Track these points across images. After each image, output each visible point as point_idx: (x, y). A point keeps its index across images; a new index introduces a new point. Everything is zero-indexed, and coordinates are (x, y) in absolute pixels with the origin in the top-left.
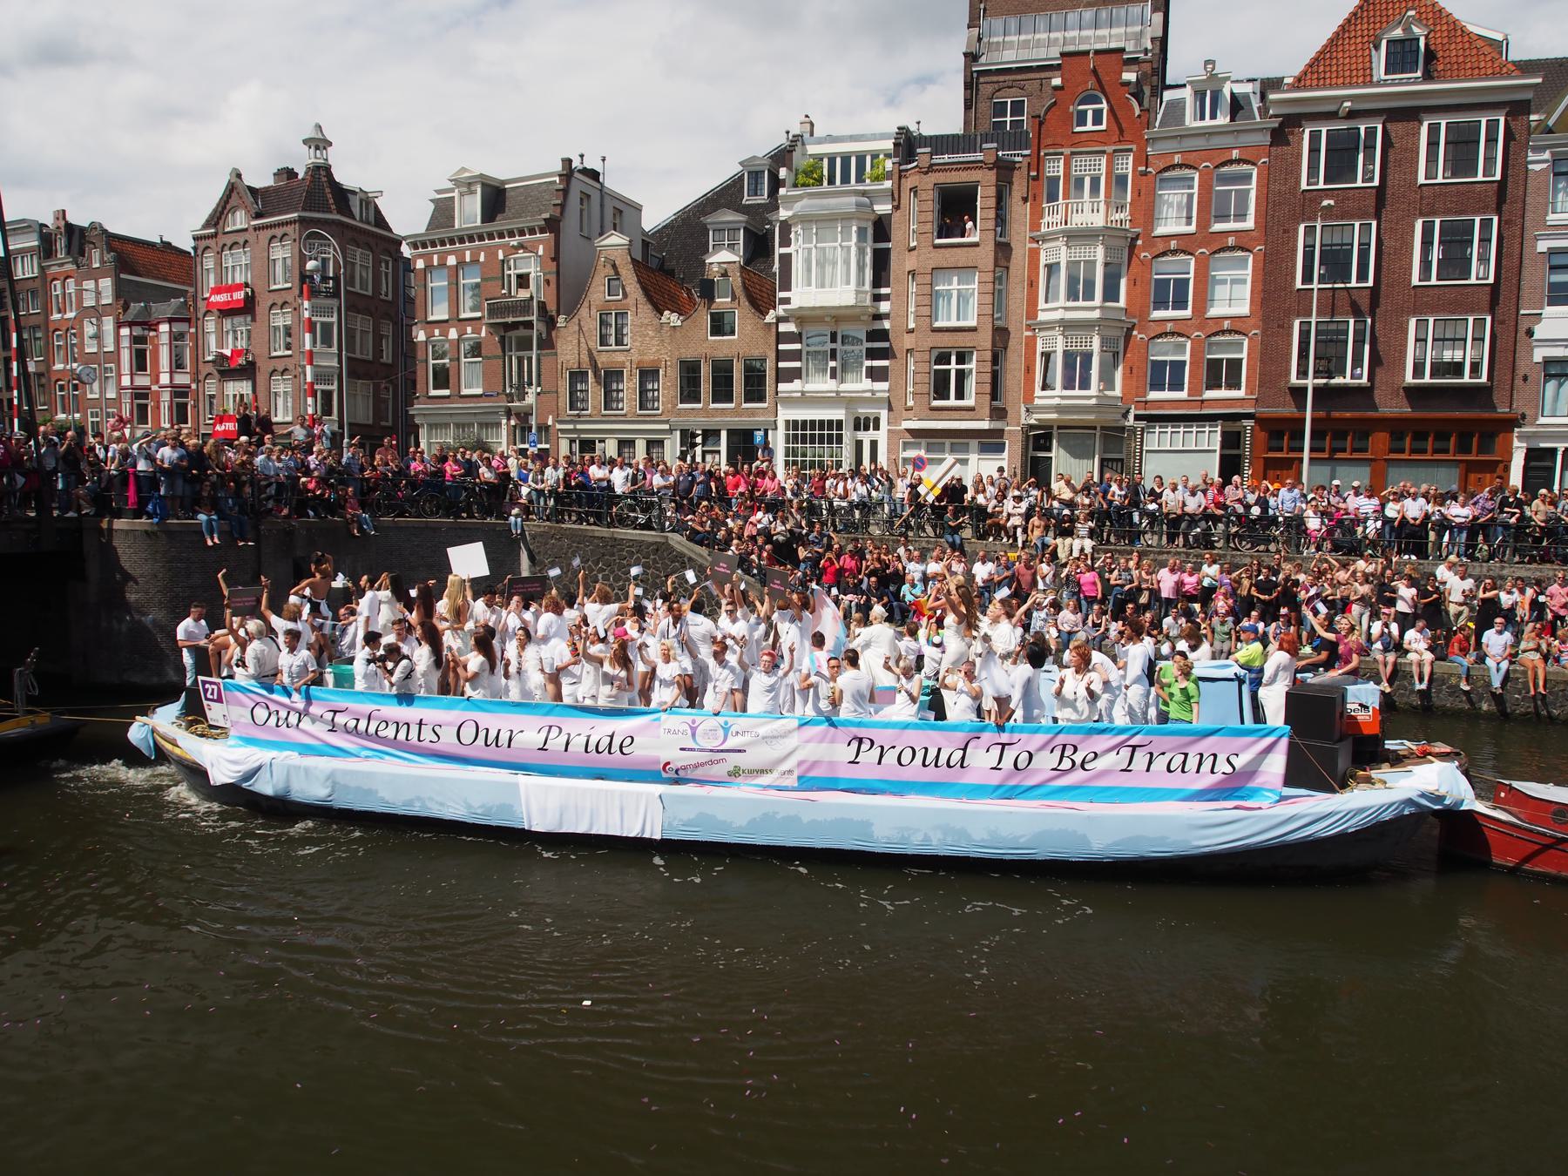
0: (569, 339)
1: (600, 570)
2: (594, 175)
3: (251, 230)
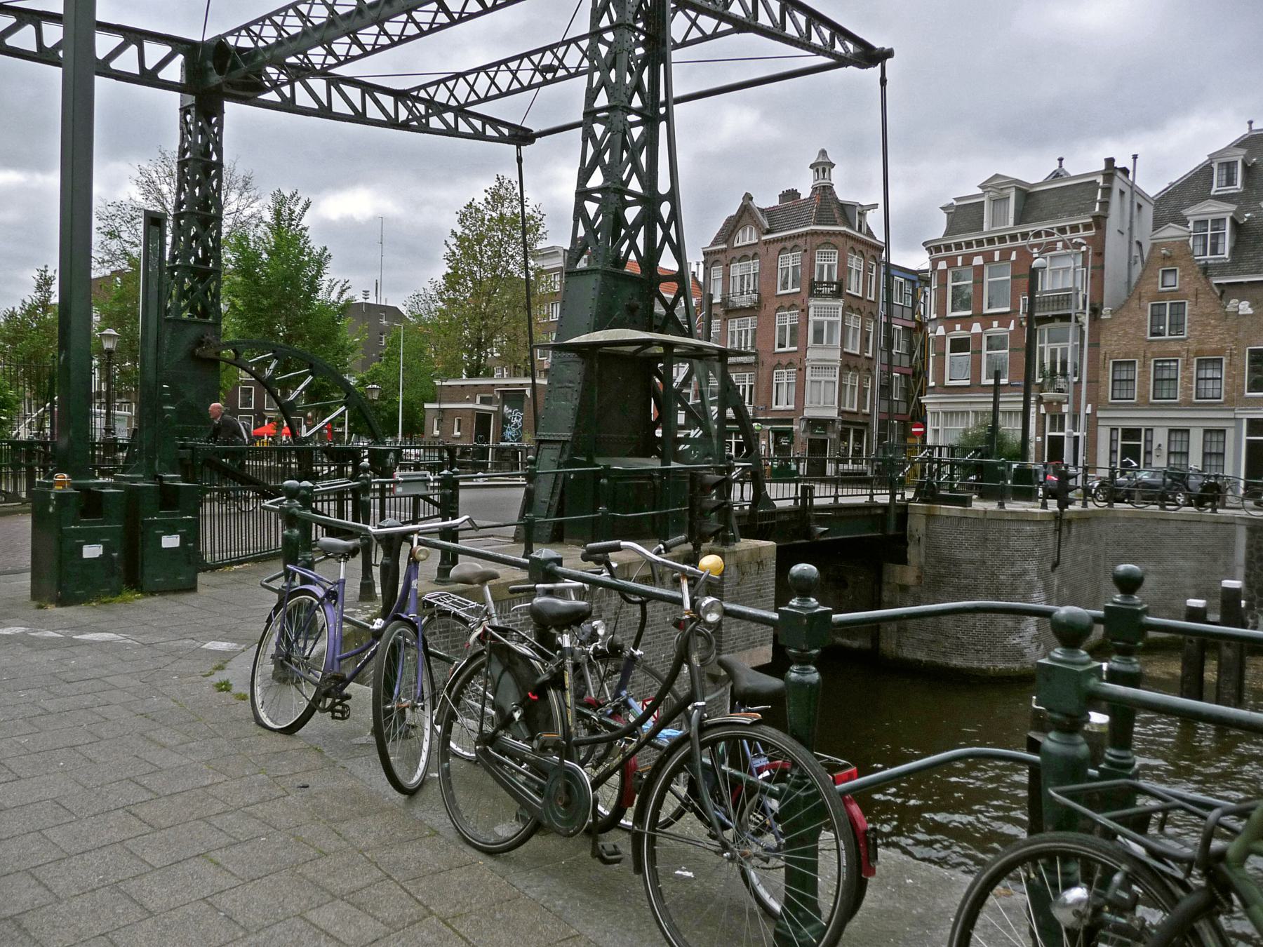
0: (1115, 330)
2: (1125, 171)
3: (761, 244)
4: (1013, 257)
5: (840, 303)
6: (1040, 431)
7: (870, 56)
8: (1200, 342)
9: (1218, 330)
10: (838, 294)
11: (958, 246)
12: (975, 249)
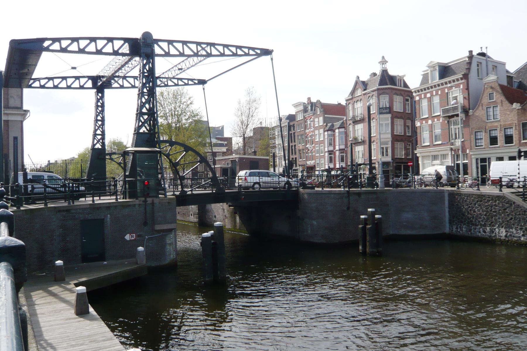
0: (474, 119)
1: (477, 208)
3: (363, 95)
4: (439, 93)
6: (453, 161)
7: (267, 52)
8: (505, 121)
9: (510, 116)
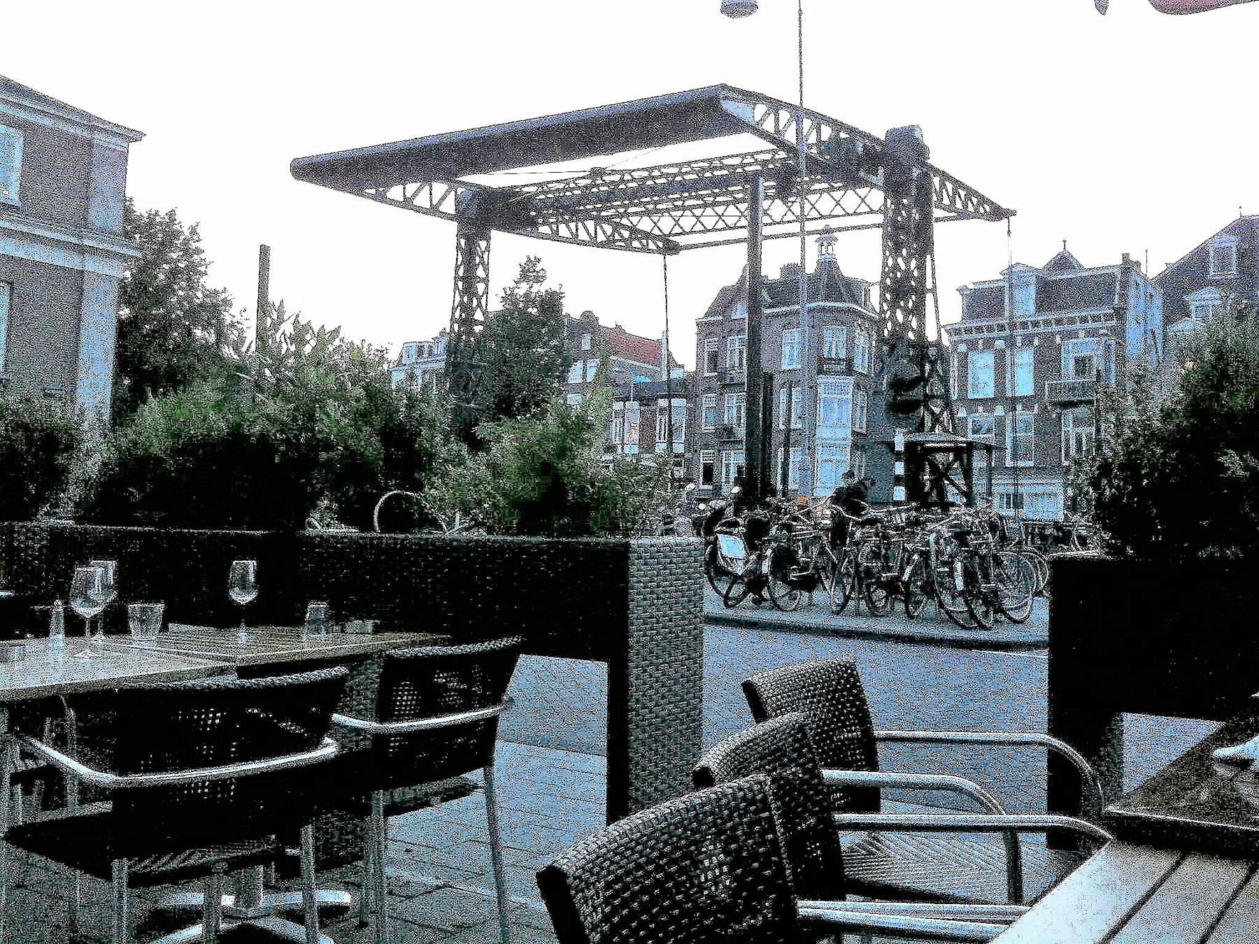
4: (1036, 342)
5: (851, 380)
7: (998, 213)
10: (849, 371)
11: (979, 329)
12: (995, 334)
